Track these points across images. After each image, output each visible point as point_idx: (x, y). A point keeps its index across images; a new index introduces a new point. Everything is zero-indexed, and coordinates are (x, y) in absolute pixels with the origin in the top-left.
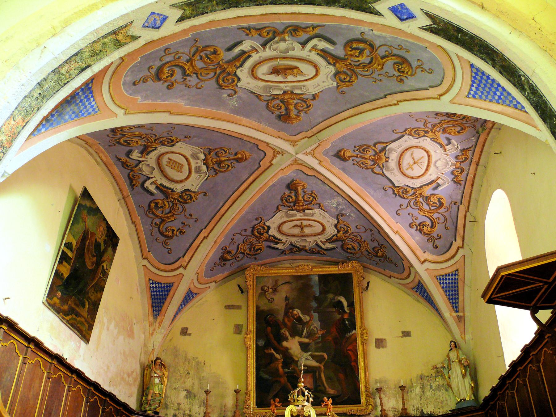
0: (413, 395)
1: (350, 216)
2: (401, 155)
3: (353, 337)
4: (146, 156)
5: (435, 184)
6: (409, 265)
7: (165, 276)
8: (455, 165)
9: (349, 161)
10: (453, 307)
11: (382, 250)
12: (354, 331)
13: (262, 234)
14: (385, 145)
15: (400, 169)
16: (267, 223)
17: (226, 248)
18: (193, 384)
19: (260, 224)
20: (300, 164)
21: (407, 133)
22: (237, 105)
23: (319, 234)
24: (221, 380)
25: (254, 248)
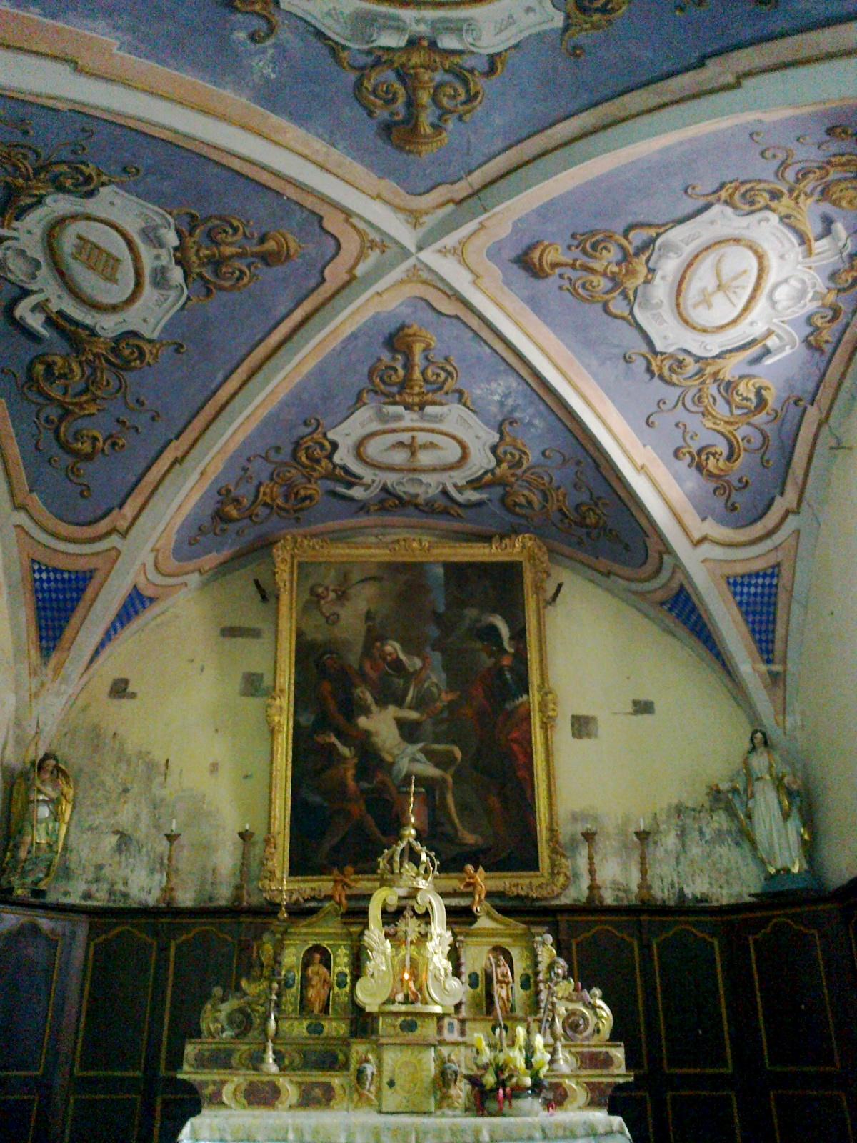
0: (660, 853)
1: (530, 424)
2: (690, 265)
3: (522, 709)
4: (15, 224)
5: (758, 350)
6: (661, 548)
8: (823, 297)
9: (551, 279)
10: (761, 651)
11: (598, 512)
12: (525, 697)
13: (318, 461)
14: (653, 232)
15: (678, 305)
16: (330, 435)
17: (229, 491)
18: (137, 817)
19: (315, 436)
20: (425, 282)
21: (723, 198)
22: (273, 76)
23: (451, 467)
24: (205, 806)
25: (297, 494)
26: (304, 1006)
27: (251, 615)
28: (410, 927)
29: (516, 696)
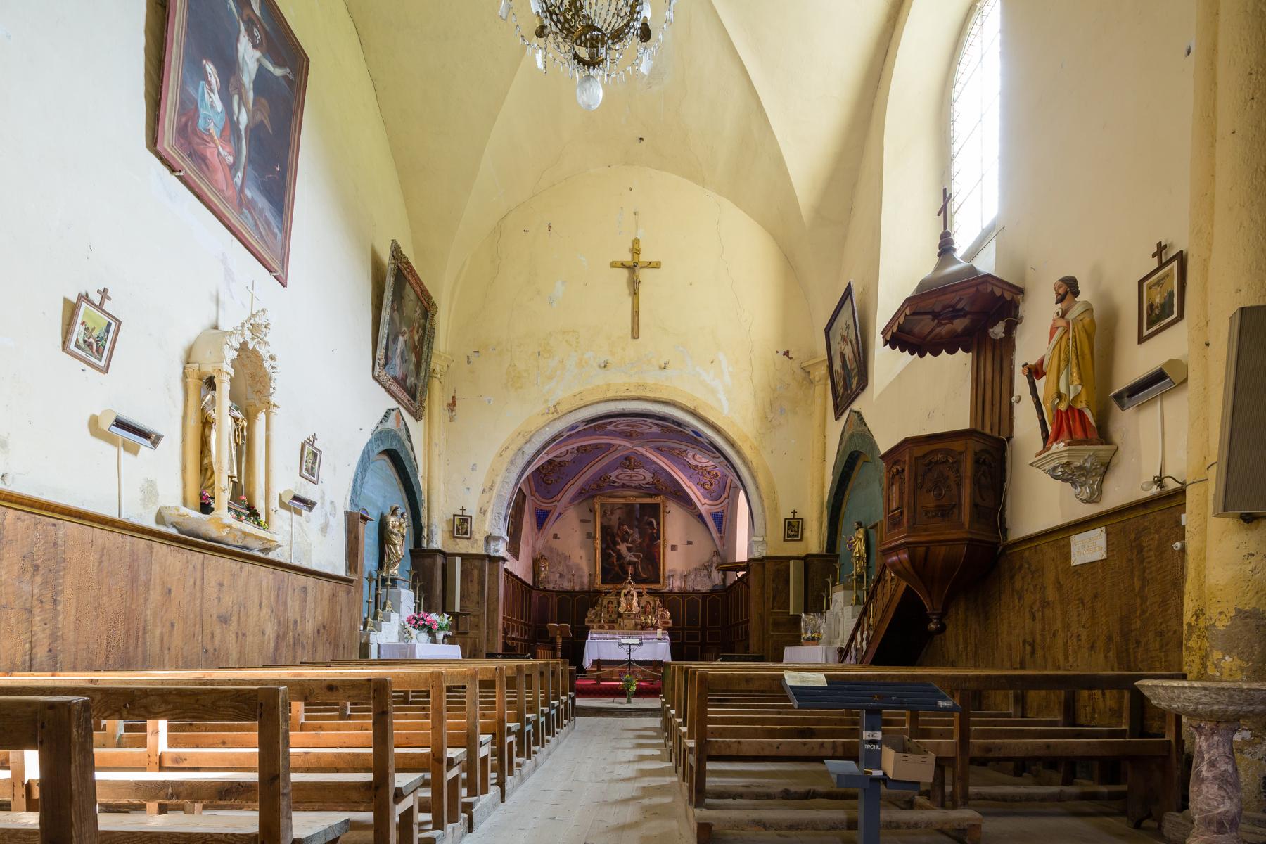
0: (690, 579)
7: (545, 506)
26: (608, 612)
27: (589, 516)
28: (630, 597)
29: (656, 541)
